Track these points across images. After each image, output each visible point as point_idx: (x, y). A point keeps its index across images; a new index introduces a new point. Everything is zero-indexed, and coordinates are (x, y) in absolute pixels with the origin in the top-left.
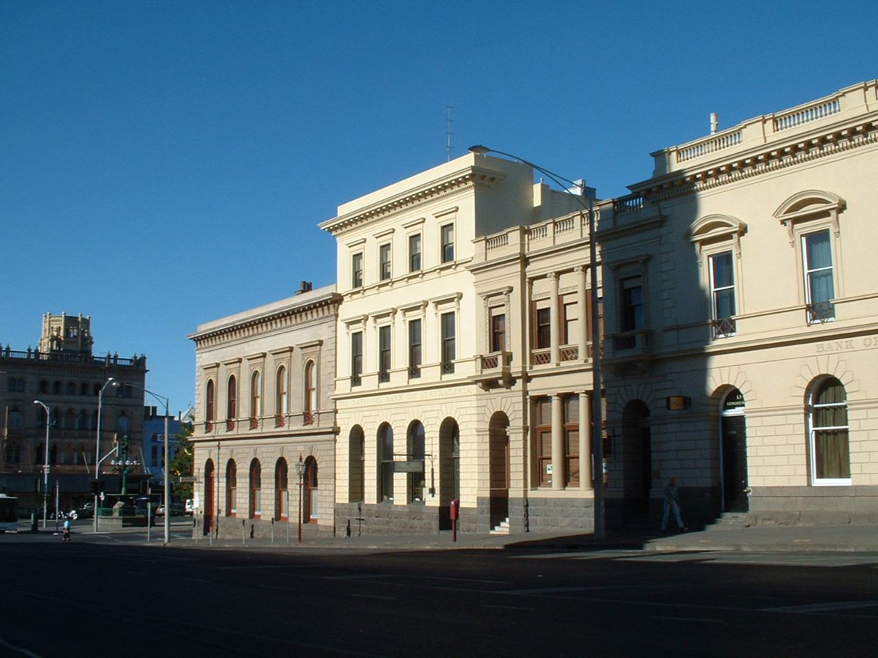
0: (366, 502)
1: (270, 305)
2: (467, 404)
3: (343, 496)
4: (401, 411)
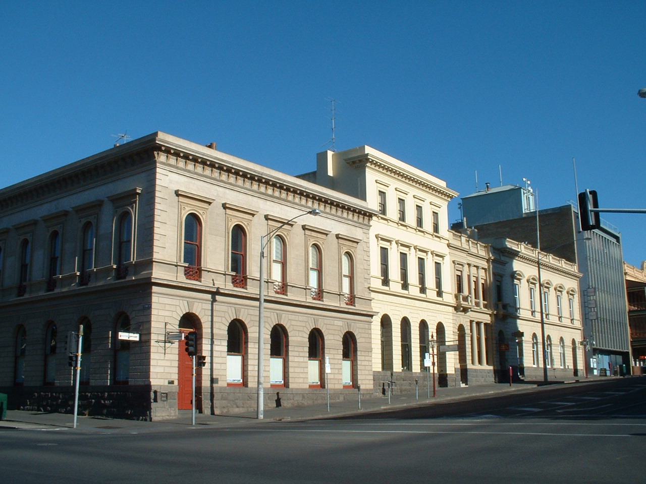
0: (414, 371)
1: (277, 172)
2: (447, 317)
3: (377, 366)
4: (416, 312)
